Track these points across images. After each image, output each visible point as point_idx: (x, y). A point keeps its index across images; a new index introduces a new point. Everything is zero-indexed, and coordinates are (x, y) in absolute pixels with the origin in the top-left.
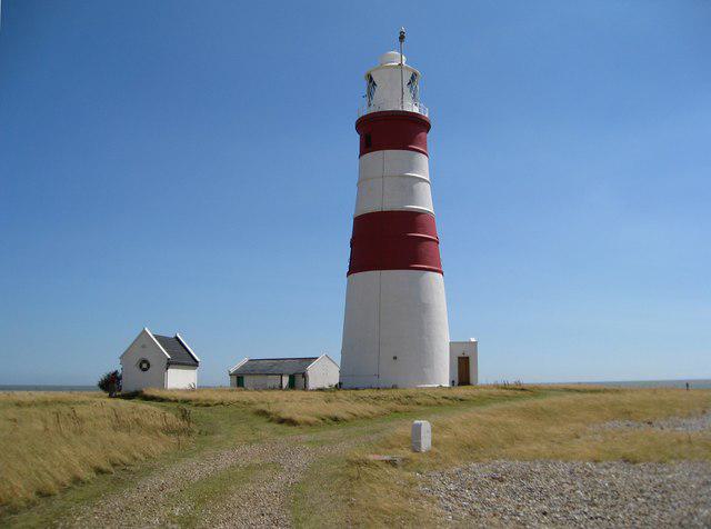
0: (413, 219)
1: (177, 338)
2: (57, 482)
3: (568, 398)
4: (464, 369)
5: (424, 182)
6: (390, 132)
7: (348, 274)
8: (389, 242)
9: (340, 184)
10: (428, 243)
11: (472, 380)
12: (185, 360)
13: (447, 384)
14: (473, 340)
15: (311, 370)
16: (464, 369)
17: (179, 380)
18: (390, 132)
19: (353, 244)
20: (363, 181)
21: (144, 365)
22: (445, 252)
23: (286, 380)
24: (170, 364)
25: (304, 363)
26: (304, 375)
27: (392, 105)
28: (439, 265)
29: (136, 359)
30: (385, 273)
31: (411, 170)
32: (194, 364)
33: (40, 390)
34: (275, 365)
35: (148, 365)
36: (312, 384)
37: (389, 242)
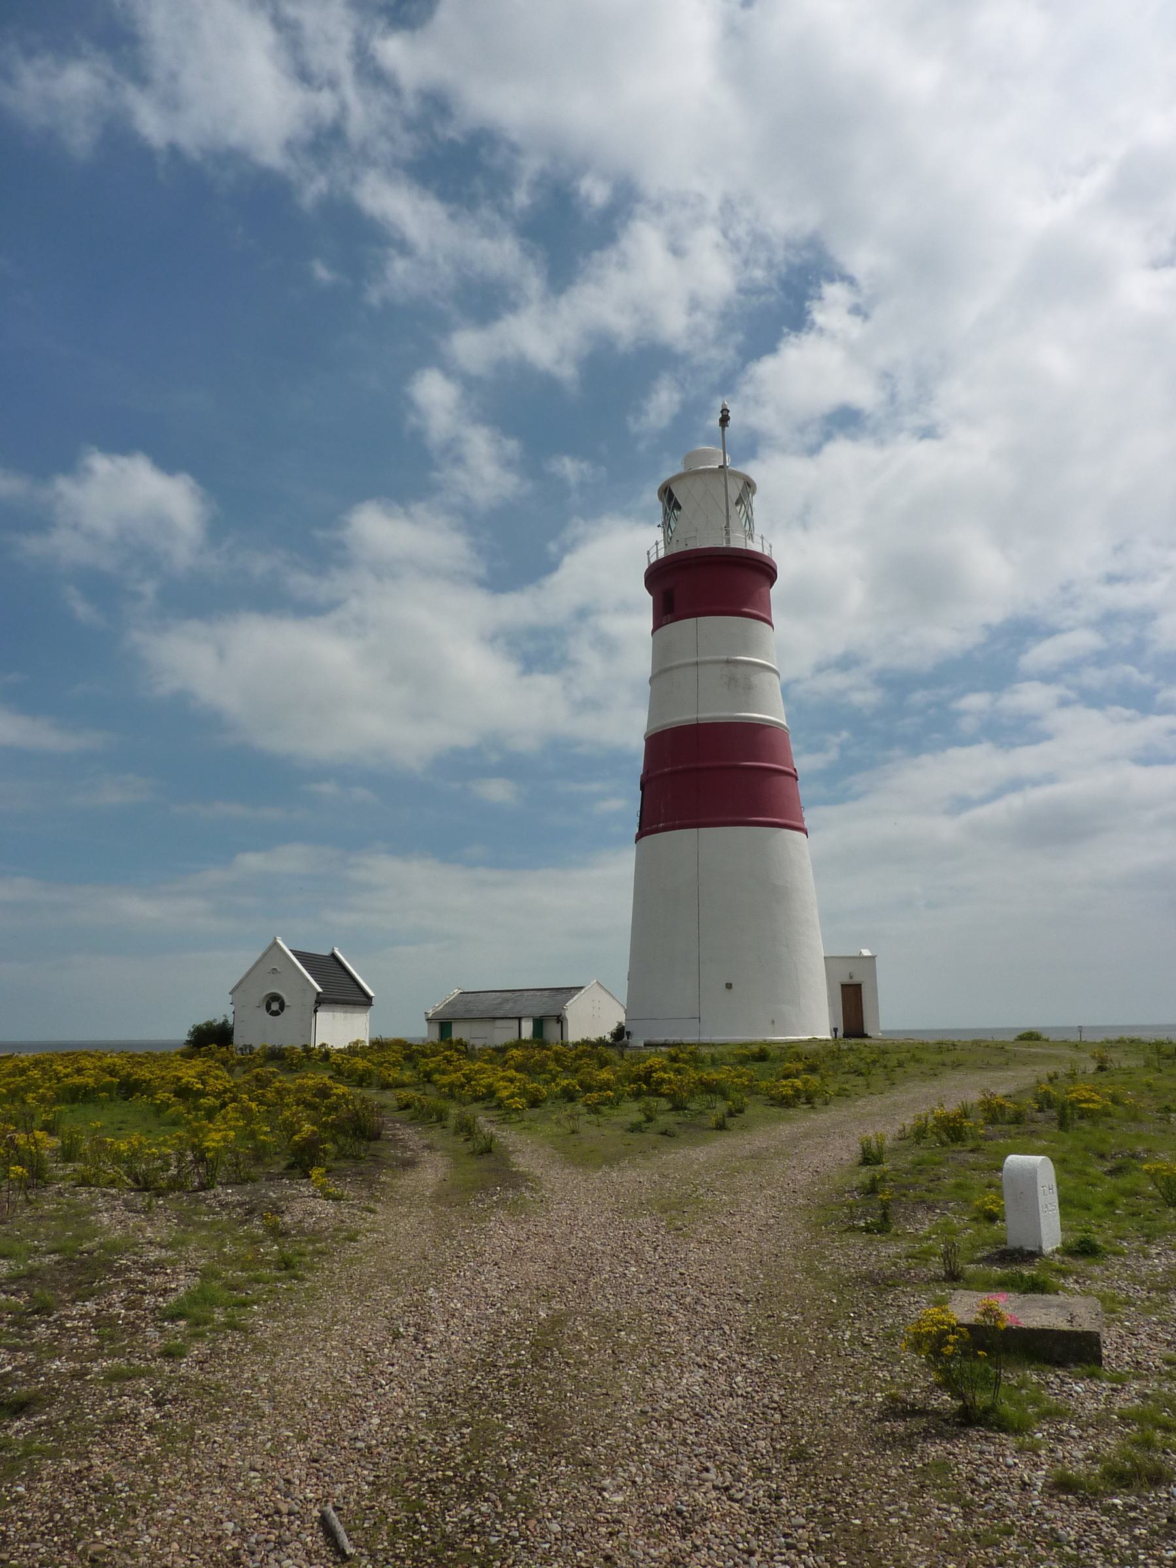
0: (752, 738)
1: (333, 955)
3: (509, 994)
4: (852, 999)
7: (639, 836)
10: (789, 778)
11: (868, 1030)
12: (341, 990)
13: (826, 1035)
14: (866, 953)
16: (852, 999)
17: (337, 1030)
19: (645, 784)
21: (275, 1004)
24: (321, 1001)
25: (560, 997)
26: (560, 1020)
28: (802, 820)
31: (746, 650)
32: (363, 1001)
34: (507, 1000)
35: (268, 1008)
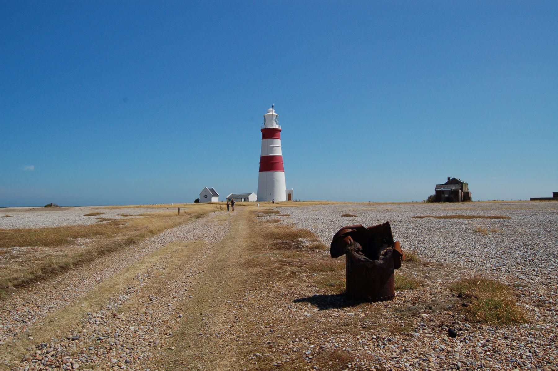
0: (273, 158)
2: (241, 265)
5: (278, 148)
6: (269, 134)
8: (269, 164)
9: (255, 150)
12: (216, 195)
15: (250, 197)
18: (269, 134)
20: (263, 146)
22: (285, 166)
23: (243, 200)
24: (213, 196)
26: (248, 198)
27: (270, 127)
29: (204, 195)
30: (268, 172)
33: (454, 218)
36: (250, 200)
37: (269, 164)
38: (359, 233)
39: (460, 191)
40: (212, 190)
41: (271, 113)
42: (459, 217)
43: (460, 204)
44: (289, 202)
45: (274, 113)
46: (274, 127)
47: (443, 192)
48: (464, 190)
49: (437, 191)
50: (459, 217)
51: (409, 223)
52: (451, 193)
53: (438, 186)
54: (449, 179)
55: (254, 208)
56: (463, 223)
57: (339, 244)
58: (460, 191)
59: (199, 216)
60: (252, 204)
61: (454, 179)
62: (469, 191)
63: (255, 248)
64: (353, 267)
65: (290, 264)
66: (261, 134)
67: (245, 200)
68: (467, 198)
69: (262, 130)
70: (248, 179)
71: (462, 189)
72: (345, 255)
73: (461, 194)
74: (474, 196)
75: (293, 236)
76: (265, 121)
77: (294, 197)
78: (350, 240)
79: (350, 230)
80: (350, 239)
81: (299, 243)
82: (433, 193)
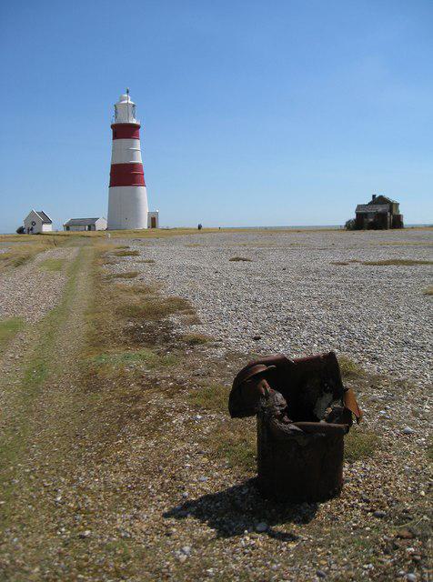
5: (139, 152)
6: (124, 132)
8: (125, 175)
12: (48, 221)
22: (148, 175)
23: (87, 227)
24: (43, 223)
36: (97, 228)
38: (281, 372)
39: (389, 214)
40: (42, 214)
41: (126, 102)
42: (396, 262)
43: (389, 231)
44: (154, 229)
45: (130, 102)
46: (131, 122)
47: (366, 215)
48: (394, 211)
49: (358, 214)
50: (396, 262)
51: (331, 274)
52: (378, 216)
53: (359, 207)
54: (374, 196)
55: (102, 245)
56: (404, 275)
57: (243, 397)
58: (389, 214)
59: (20, 263)
60: (101, 237)
61: (381, 197)
62: (401, 213)
63: (97, 342)
64: (270, 440)
65: (156, 386)
66: (110, 132)
67: (89, 229)
68: (397, 223)
69: (113, 127)
70: (94, 201)
71: (391, 211)
72: (254, 419)
73: (390, 218)
74: (406, 222)
75: (157, 312)
76: (116, 112)
77: (161, 224)
78: (264, 387)
79: (262, 369)
80: (265, 386)
81: (169, 327)
82: (353, 216)
